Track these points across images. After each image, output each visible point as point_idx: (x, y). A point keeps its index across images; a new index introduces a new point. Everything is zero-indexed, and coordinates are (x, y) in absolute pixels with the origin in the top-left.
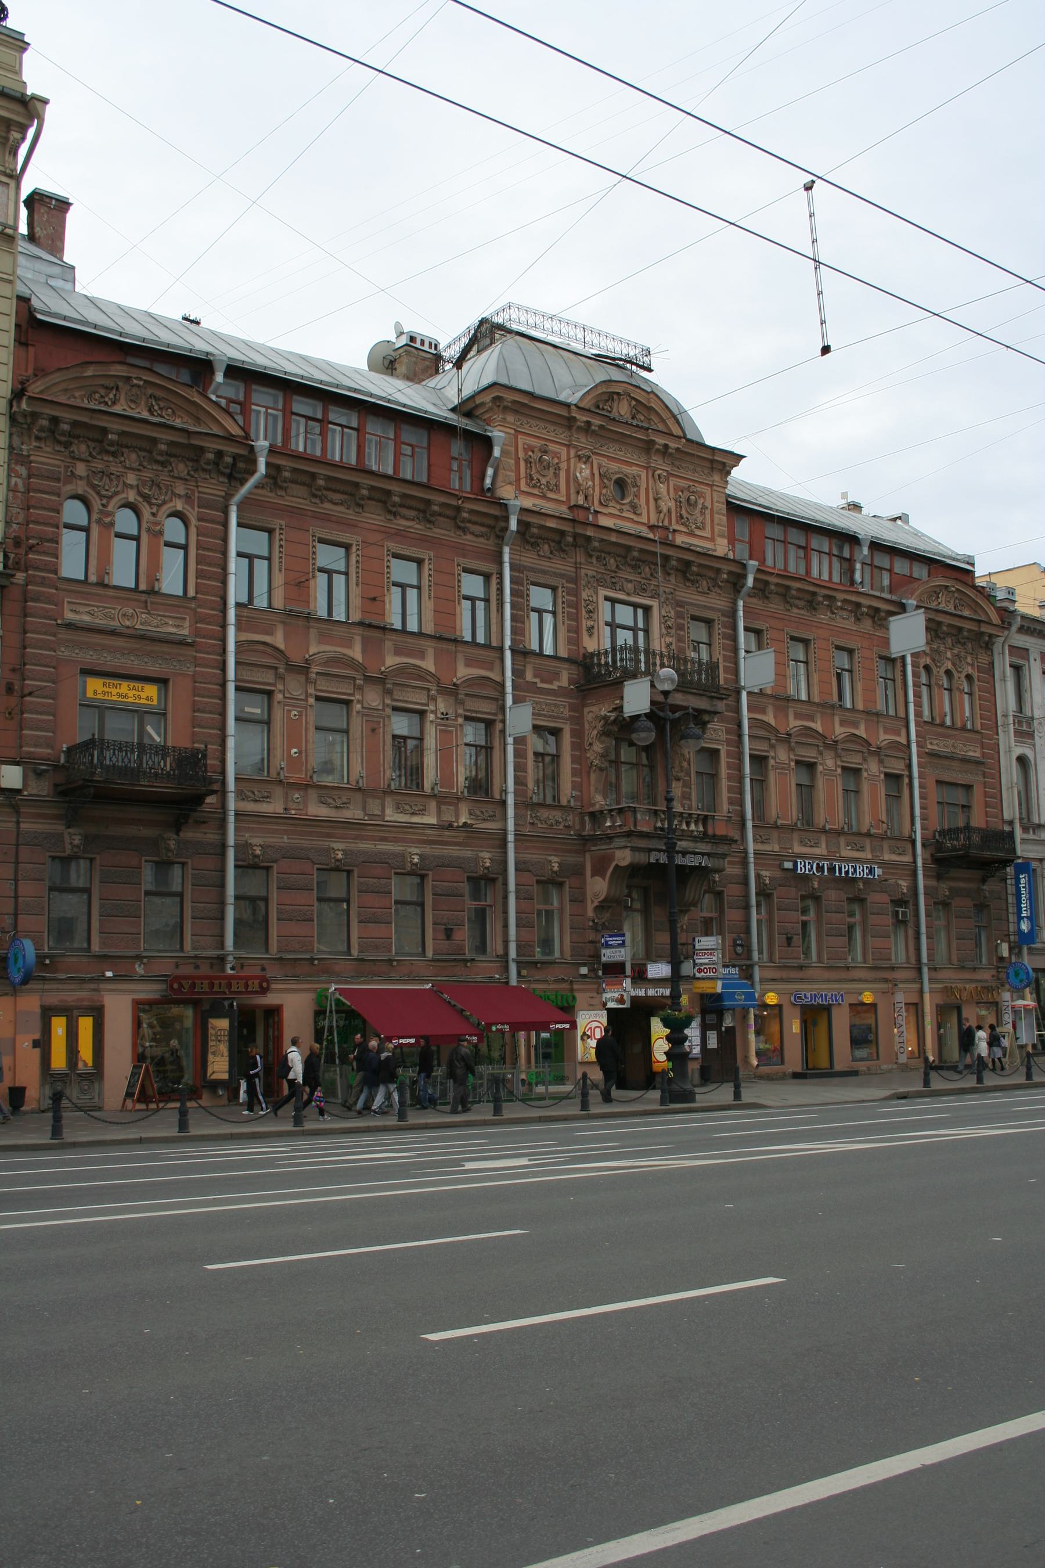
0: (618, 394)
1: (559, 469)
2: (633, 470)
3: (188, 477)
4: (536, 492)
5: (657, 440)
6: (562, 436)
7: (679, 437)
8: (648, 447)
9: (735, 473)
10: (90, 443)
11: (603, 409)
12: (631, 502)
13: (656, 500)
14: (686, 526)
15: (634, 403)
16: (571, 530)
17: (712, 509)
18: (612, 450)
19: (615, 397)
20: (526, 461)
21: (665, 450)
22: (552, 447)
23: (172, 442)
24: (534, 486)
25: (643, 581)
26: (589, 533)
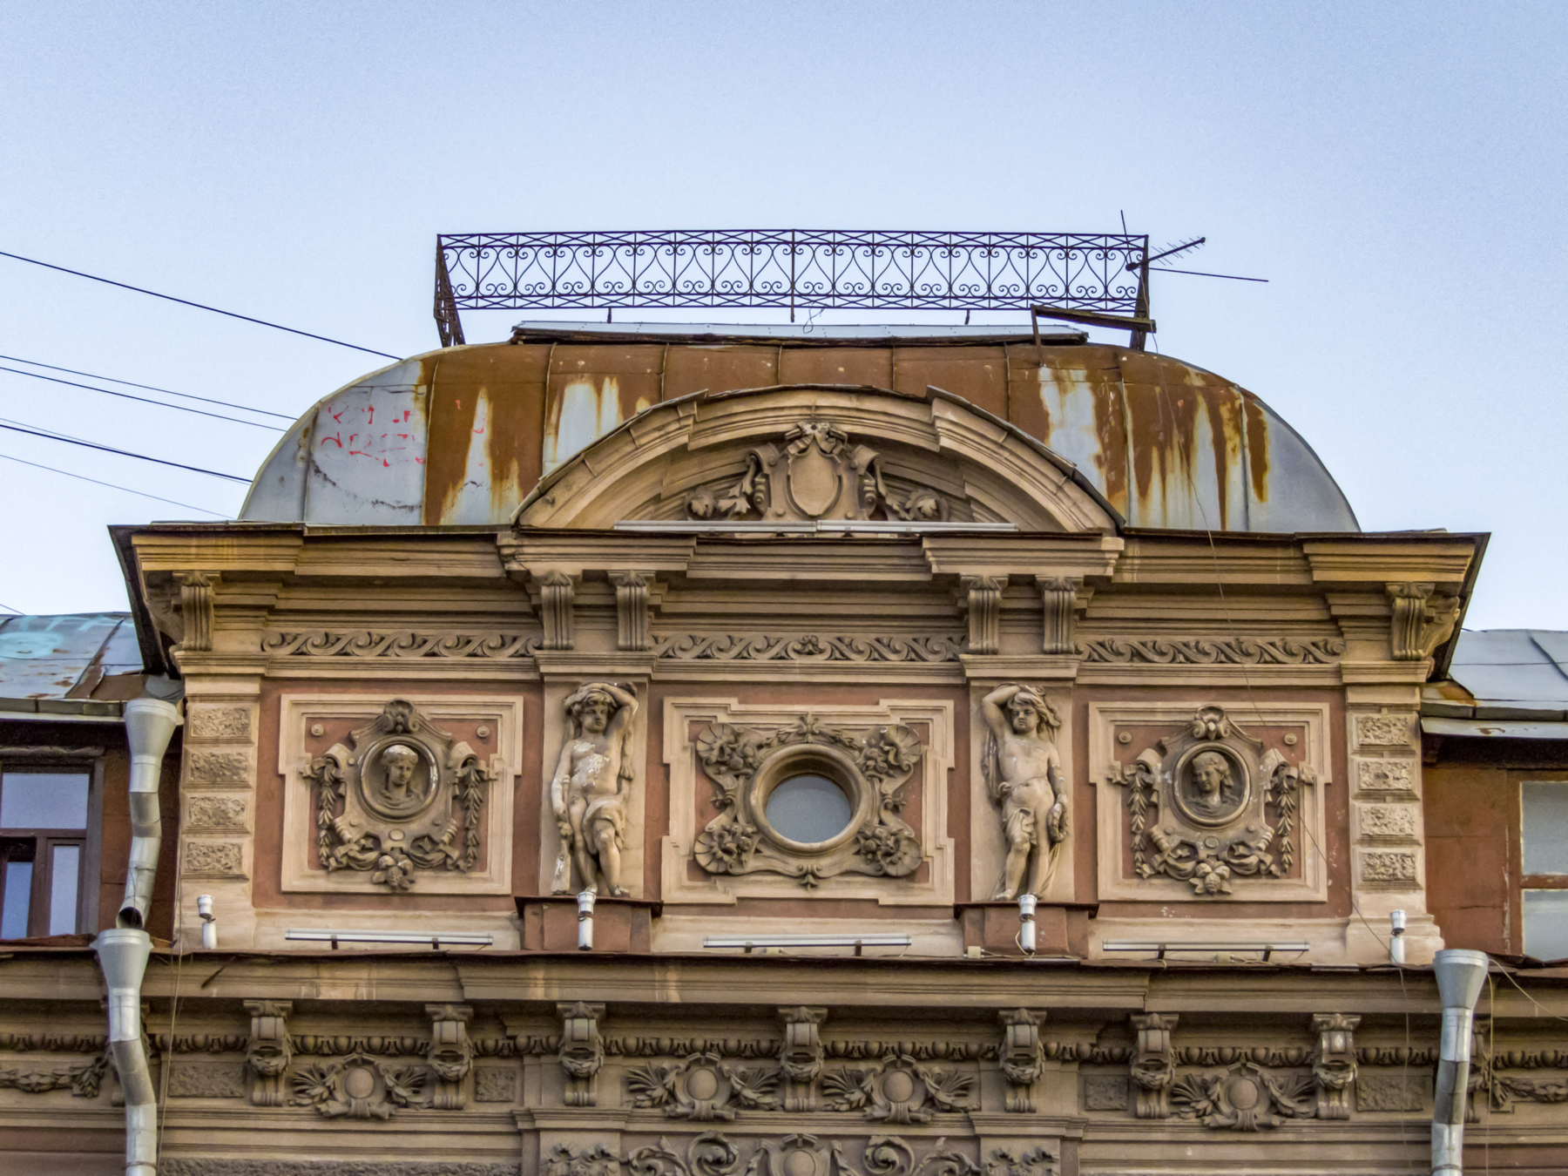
0: (779, 440)
1: (483, 780)
2: (889, 712)
3: (728, 1113)
4: (359, 883)
5: (965, 571)
6: (504, 657)
7: (1092, 536)
8: (948, 606)
9: (1486, 611)
10: (1266, 1074)
11: (718, 514)
12: (860, 836)
13: (999, 801)
14: (1182, 877)
15: (865, 455)
16: (449, 994)
17: (1338, 791)
18: (760, 650)
19: (766, 454)
20: (315, 781)
21: (1028, 604)
22: (427, 704)
23: (832, 1009)
24: (350, 866)
25: (880, 1133)
26: (538, 993)
